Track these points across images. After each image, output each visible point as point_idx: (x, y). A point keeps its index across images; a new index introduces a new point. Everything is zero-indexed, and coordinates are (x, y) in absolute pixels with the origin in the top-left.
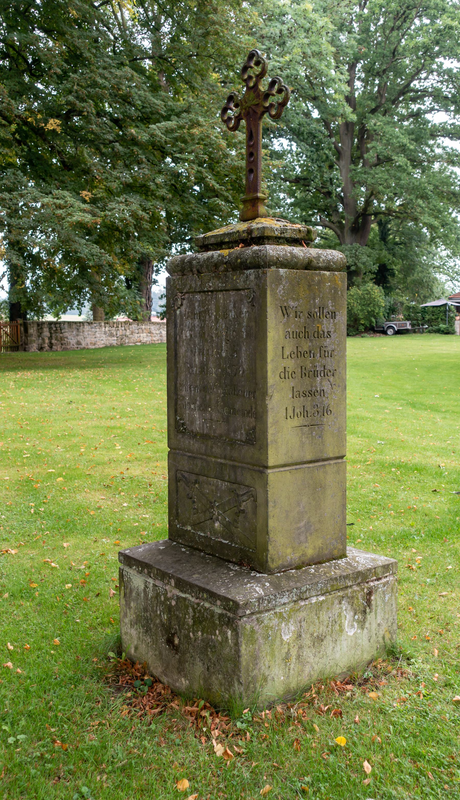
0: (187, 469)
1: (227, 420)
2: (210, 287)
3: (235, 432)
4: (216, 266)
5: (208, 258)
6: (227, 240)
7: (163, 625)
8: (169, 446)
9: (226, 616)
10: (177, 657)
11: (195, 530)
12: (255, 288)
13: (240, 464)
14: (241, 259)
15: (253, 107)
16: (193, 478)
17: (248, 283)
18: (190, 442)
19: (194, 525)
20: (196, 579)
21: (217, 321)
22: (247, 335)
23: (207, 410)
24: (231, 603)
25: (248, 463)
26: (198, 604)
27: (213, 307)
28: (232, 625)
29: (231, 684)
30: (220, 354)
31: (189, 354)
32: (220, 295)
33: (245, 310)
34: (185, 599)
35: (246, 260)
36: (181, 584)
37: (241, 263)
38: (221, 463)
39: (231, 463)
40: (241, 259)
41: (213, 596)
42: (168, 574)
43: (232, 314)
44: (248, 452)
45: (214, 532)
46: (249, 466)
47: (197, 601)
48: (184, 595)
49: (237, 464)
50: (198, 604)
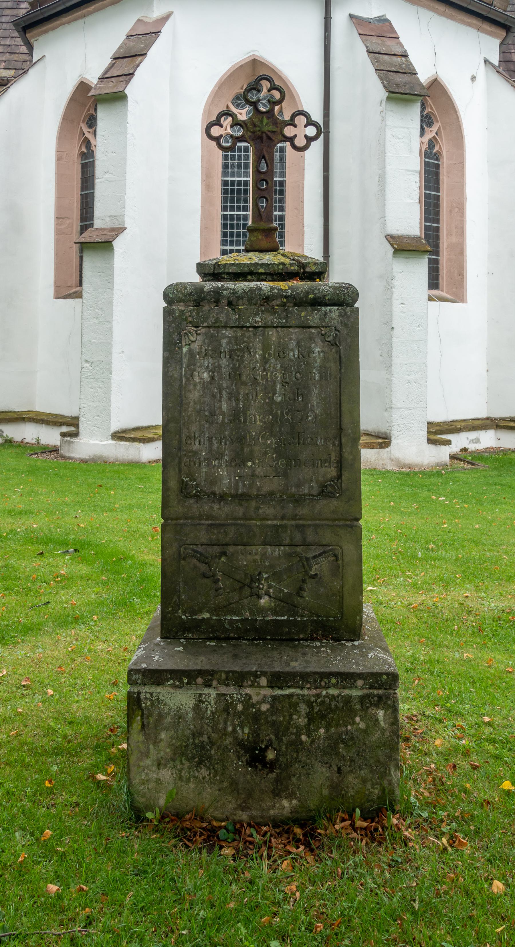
0: (204, 541)
1: (285, 475)
2: (257, 322)
3: (298, 486)
4: (267, 299)
5: (251, 290)
6: (261, 270)
7: (240, 743)
8: (163, 518)
9: (375, 696)
10: (272, 776)
11: (218, 615)
12: (339, 327)
13: (310, 522)
14: (314, 294)
15: (269, 133)
16: (216, 549)
17: (327, 320)
18: (211, 507)
19: (216, 610)
20: (297, 666)
21: (265, 360)
22: (321, 377)
23: (245, 465)
24: (385, 677)
25: (328, 519)
26: (318, 696)
27: (258, 345)
28: (385, 703)
29: (384, 774)
30: (272, 399)
31: (208, 399)
32: (272, 333)
33: (318, 349)
34: (291, 696)
35: (324, 296)
36: (277, 680)
37: (314, 299)
38: (275, 526)
39: (293, 523)
40: (314, 294)
41: (347, 678)
42: (250, 673)
43: (294, 354)
44: (329, 506)
45: (261, 611)
46: (326, 522)
47: (313, 692)
48: (287, 692)
49: (301, 522)
50: (318, 696)
